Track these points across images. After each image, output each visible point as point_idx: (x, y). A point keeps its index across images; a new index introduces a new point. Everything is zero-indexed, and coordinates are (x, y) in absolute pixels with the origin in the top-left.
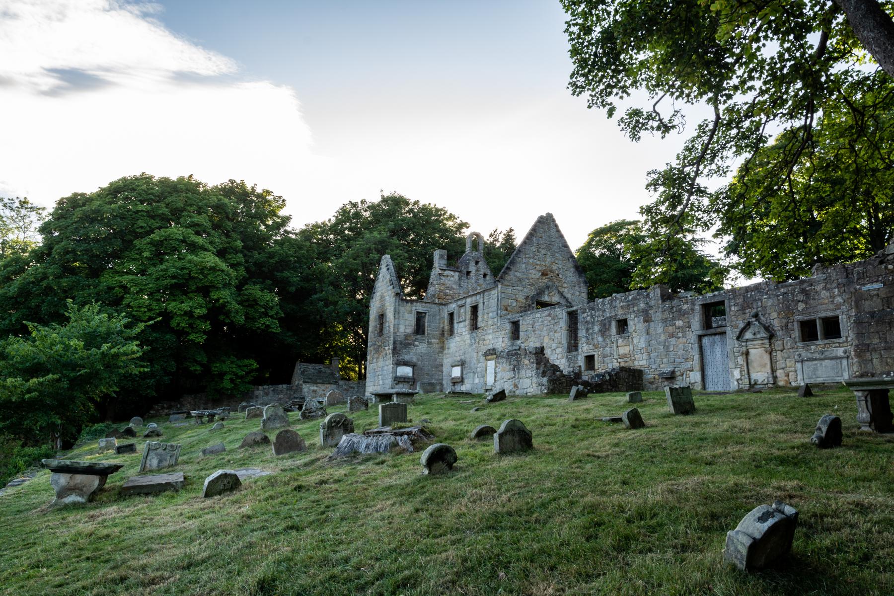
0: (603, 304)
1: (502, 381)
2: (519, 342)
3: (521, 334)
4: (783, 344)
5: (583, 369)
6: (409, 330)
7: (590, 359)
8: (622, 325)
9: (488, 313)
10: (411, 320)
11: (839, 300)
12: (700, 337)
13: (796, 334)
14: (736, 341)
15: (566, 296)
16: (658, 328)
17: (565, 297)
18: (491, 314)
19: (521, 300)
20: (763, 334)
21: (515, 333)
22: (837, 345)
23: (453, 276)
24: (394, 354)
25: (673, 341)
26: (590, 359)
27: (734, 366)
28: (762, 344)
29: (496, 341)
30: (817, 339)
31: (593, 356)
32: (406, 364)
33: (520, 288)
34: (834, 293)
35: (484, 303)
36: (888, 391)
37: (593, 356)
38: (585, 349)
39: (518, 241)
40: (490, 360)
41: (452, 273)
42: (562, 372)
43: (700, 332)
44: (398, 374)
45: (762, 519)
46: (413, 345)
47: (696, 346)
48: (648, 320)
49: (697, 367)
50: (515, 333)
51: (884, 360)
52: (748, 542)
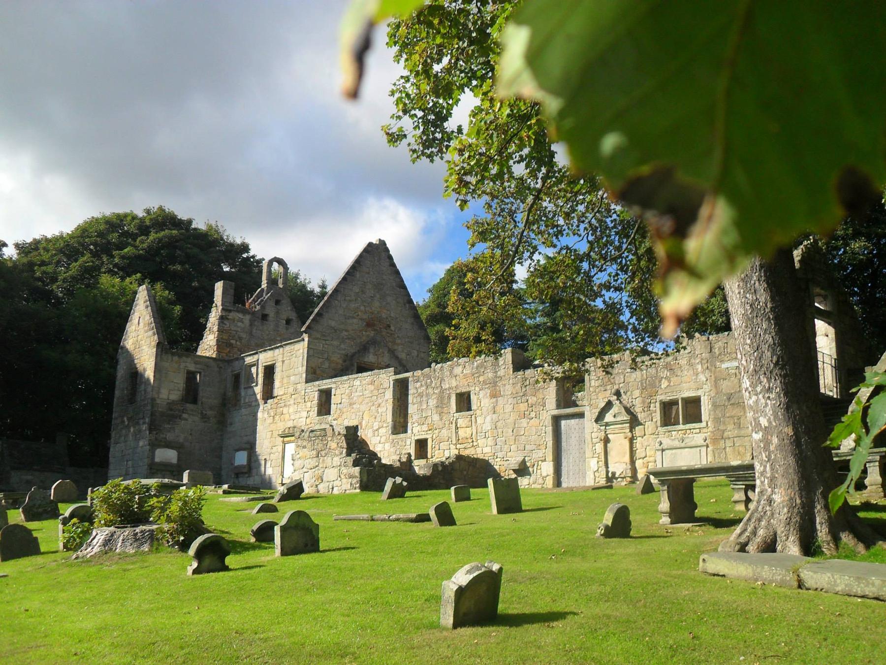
0: (442, 368)
1: (302, 471)
2: (330, 418)
3: (333, 407)
4: (644, 428)
5: (413, 454)
6: (175, 396)
7: (422, 446)
8: (464, 402)
9: (289, 377)
10: (179, 381)
11: (702, 378)
12: (557, 420)
13: (657, 416)
14: (594, 423)
15: (400, 356)
16: (506, 404)
17: (397, 358)
18: (292, 378)
19: (335, 359)
20: (626, 417)
21: (325, 404)
22: (698, 431)
23: (241, 321)
24: (150, 430)
25: (524, 422)
26: (422, 446)
27: (591, 455)
28: (622, 428)
29: (298, 416)
30: (679, 424)
31: (426, 440)
32: (169, 445)
33: (335, 343)
34: (697, 369)
35: (283, 361)
36: (693, 480)
37: (426, 440)
38: (416, 431)
39: (330, 289)
40: (289, 442)
41: (240, 316)
42: (380, 459)
43: (556, 412)
44: (157, 460)
45: (469, 572)
46: (180, 417)
47: (550, 429)
48: (494, 395)
49: (550, 457)
50: (325, 404)
51: (736, 449)
52: (455, 588)
